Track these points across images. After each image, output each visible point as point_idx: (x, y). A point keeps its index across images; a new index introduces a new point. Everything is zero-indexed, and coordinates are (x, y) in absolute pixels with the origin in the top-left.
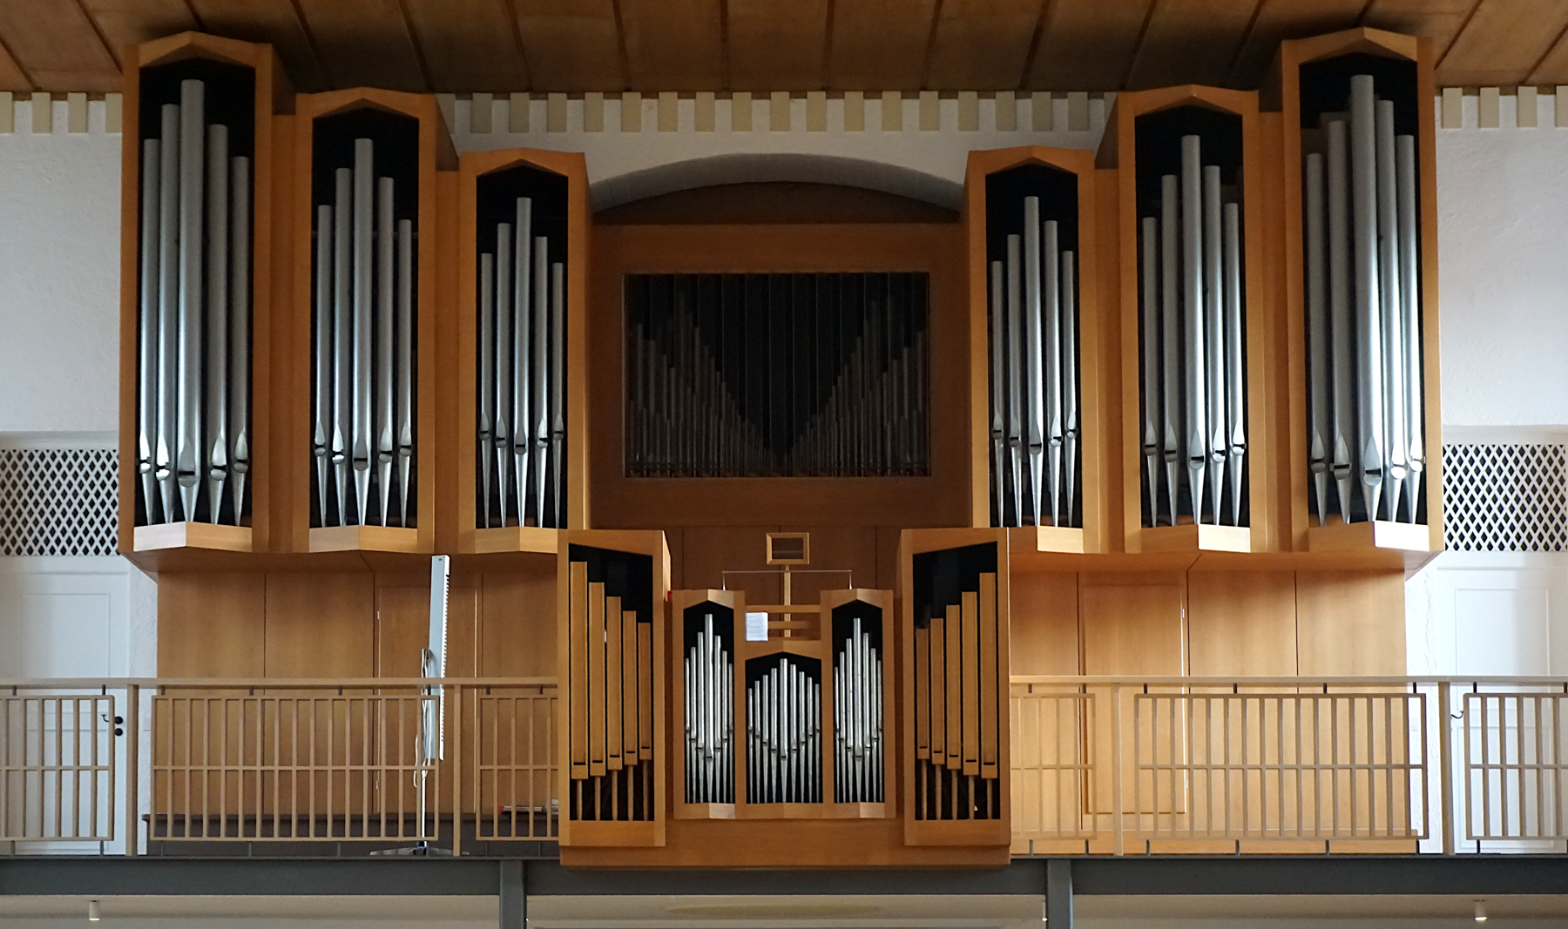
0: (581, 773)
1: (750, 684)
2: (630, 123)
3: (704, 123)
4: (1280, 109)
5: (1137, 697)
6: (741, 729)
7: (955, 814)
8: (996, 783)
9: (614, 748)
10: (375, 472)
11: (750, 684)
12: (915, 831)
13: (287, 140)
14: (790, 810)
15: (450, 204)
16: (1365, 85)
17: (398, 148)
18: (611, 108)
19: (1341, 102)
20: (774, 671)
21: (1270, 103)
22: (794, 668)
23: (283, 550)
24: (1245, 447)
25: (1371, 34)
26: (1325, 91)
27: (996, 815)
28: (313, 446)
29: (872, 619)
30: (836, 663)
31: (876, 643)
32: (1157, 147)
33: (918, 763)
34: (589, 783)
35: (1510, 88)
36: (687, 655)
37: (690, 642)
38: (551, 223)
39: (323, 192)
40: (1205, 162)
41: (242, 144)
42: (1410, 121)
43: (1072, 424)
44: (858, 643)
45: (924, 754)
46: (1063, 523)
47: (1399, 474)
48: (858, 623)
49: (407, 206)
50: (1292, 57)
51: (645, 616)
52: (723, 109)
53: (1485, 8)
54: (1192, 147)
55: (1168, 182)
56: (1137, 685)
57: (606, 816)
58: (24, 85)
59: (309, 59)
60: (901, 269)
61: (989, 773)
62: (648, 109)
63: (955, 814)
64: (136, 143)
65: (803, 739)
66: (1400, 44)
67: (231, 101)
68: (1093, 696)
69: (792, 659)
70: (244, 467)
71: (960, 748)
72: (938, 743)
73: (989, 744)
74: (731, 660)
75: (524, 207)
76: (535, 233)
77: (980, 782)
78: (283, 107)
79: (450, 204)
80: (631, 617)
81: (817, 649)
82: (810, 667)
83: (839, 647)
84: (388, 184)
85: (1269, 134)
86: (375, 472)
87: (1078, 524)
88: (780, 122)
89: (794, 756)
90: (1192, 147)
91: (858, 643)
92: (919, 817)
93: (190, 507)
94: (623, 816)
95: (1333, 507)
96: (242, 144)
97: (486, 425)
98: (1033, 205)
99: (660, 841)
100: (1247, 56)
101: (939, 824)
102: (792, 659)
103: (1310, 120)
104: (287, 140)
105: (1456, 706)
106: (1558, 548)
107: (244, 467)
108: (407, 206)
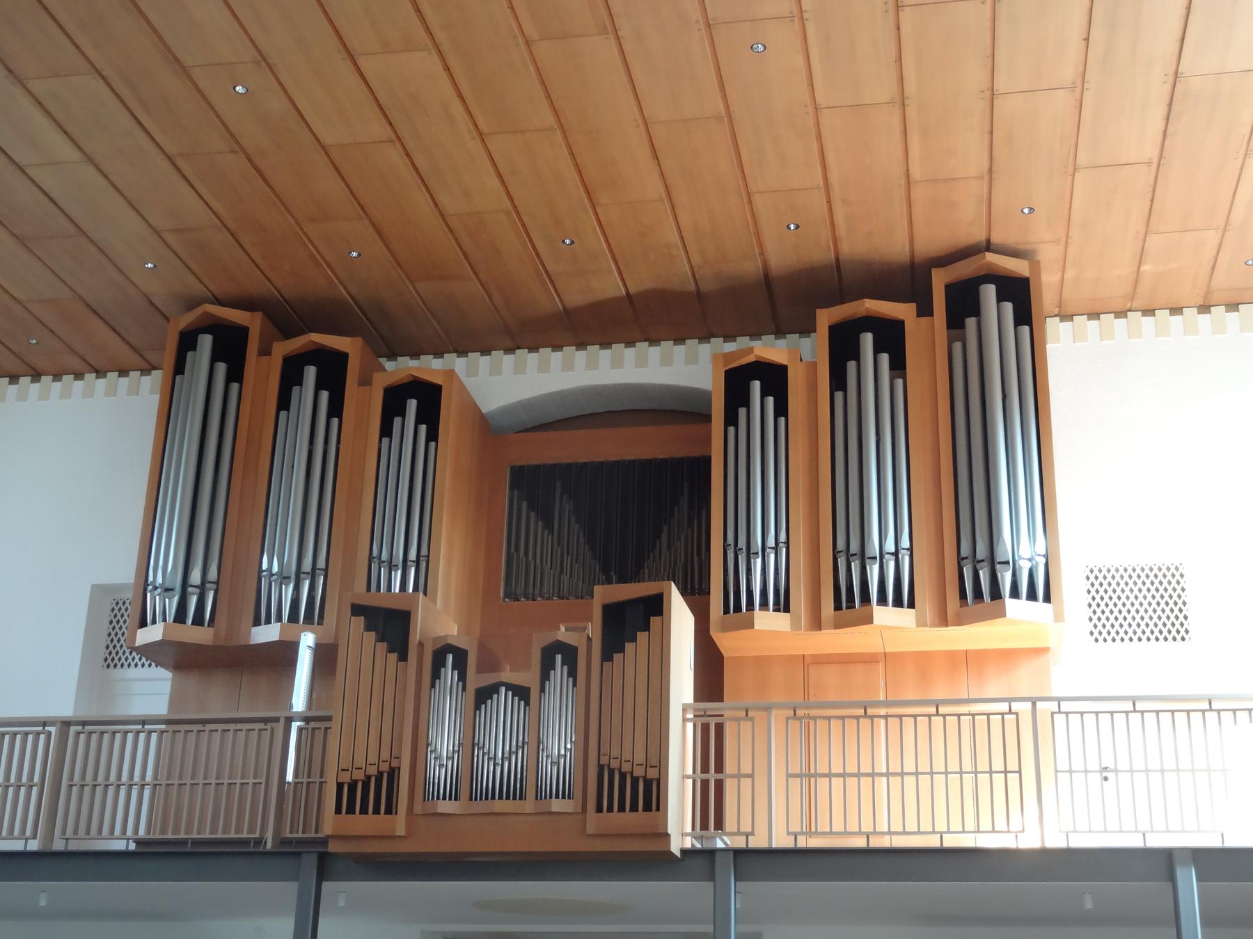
0: (345, 778)
1: (477, 708)
2: (520, 369)
3: (568, 366)
4: (931, 314)
5: (788, 719)
6: (470, 745)
7: (190, 620)
8: (658, 781)
9: (373, 758)
10: (297, 589)
11: (477, 708)
12: (594, 821)
13: (263, 372)
14: (499, 805)
15: (365, 403)
16: (989, 292)
17: (333, 371)
18: (508, 360)
19: (975, 309)
20: (495, 696)
21: (925, 310)
22: (510, 693)
23: (234, 643)
24: (911, 550)
25: (990, 257)
26: (963, 304)
27: (658, 809)
28: (260, 570)
29: (570, 654)
30: (542, 690)
31: (573, 673)
32: (843, 347)
33: (601, 768)
34: (353, 786)
35: (1121, 314)
36: (433, 686)
37: (436, 675)
38: (430, 416)
39: (284, 403)
40: (877, 351)
41: (236, 375)
42: (1024, 316)
43: (783, 538)
44: (559, 672)
45: (604, 760)
46: (777, 610)
47: (1025, 566)
48: (559, 658)
49: (336, 409)
50: (939, 280)
51: (403, 657)
52: (580, 356)
53: (806, 3)
54: (867, 340)
55: (852, 365)
56: (788, 708)
57: (364, 811)
58: (145, 365)
59: (286, 317)
60: (696, 455)
61: (652, 774)
62: (532, 359)
63: (190, 620)
64: (170, 377)
65: (514, 749)
66: (1018, 267)
67: (231, 347)
68: (752, 719)
69: (509, 687)
70: (214, 586)
71: (631, 756)
72: (615, 753)
73: (653, 750)
74: (464, 689)
75: (412, 405)
76: (418, 422)
77: (648, 783)
78: (265, 351)
79: (365, 403)
80: (393, 657)
81: (528, 678)
82: (522, 693)
83: (545, 677)
84: (325, 395)
85: (924, 335)
86: (297, 589)
87: (787, 610)
88: (617, 363)
89: (506, 764)
90: (867, 340)
91: (559, 672)
92: (599, 809)
93: (171, 616)
94: (377, 811)
95: (978, 595)
96: (236, 375)
97: (375, 553)
98: (756, 386)
99: (401, 831)
100: (910, 280)
101: (616, 816)
102: (509, 687)
103: (955, 322)
104: (263, 372)
105: (1044, 720)
106: (1183, 639)
107: (214, 586)
108: (336, 409)
